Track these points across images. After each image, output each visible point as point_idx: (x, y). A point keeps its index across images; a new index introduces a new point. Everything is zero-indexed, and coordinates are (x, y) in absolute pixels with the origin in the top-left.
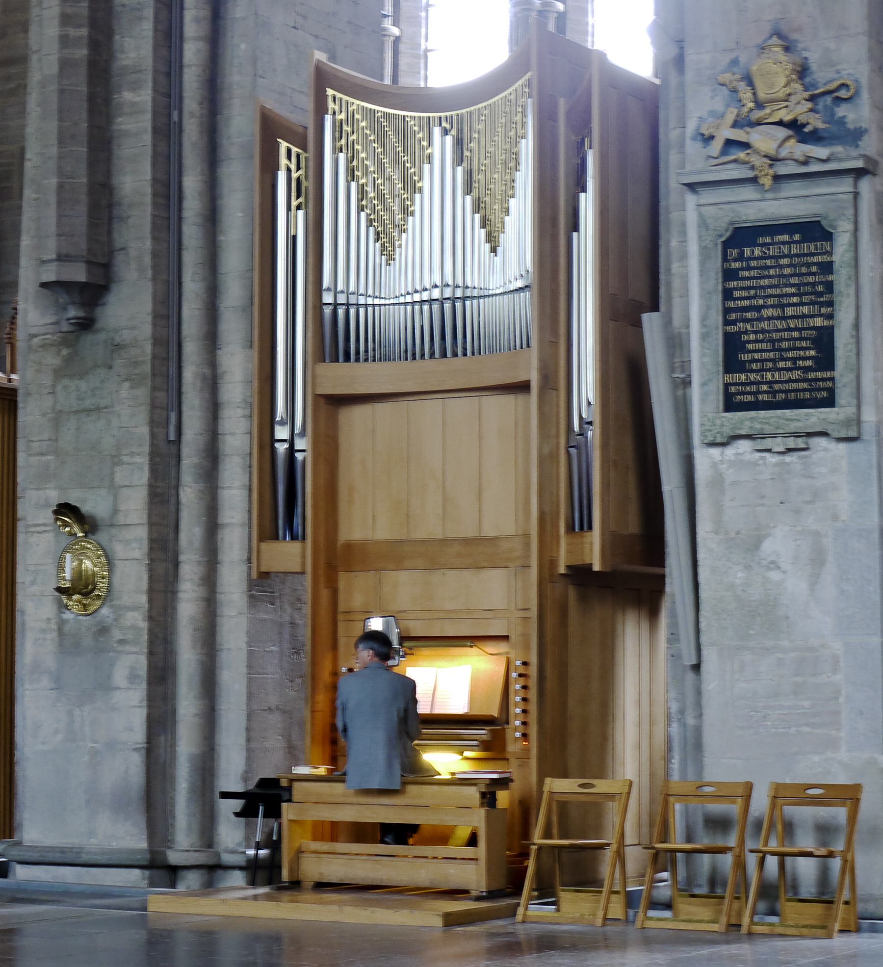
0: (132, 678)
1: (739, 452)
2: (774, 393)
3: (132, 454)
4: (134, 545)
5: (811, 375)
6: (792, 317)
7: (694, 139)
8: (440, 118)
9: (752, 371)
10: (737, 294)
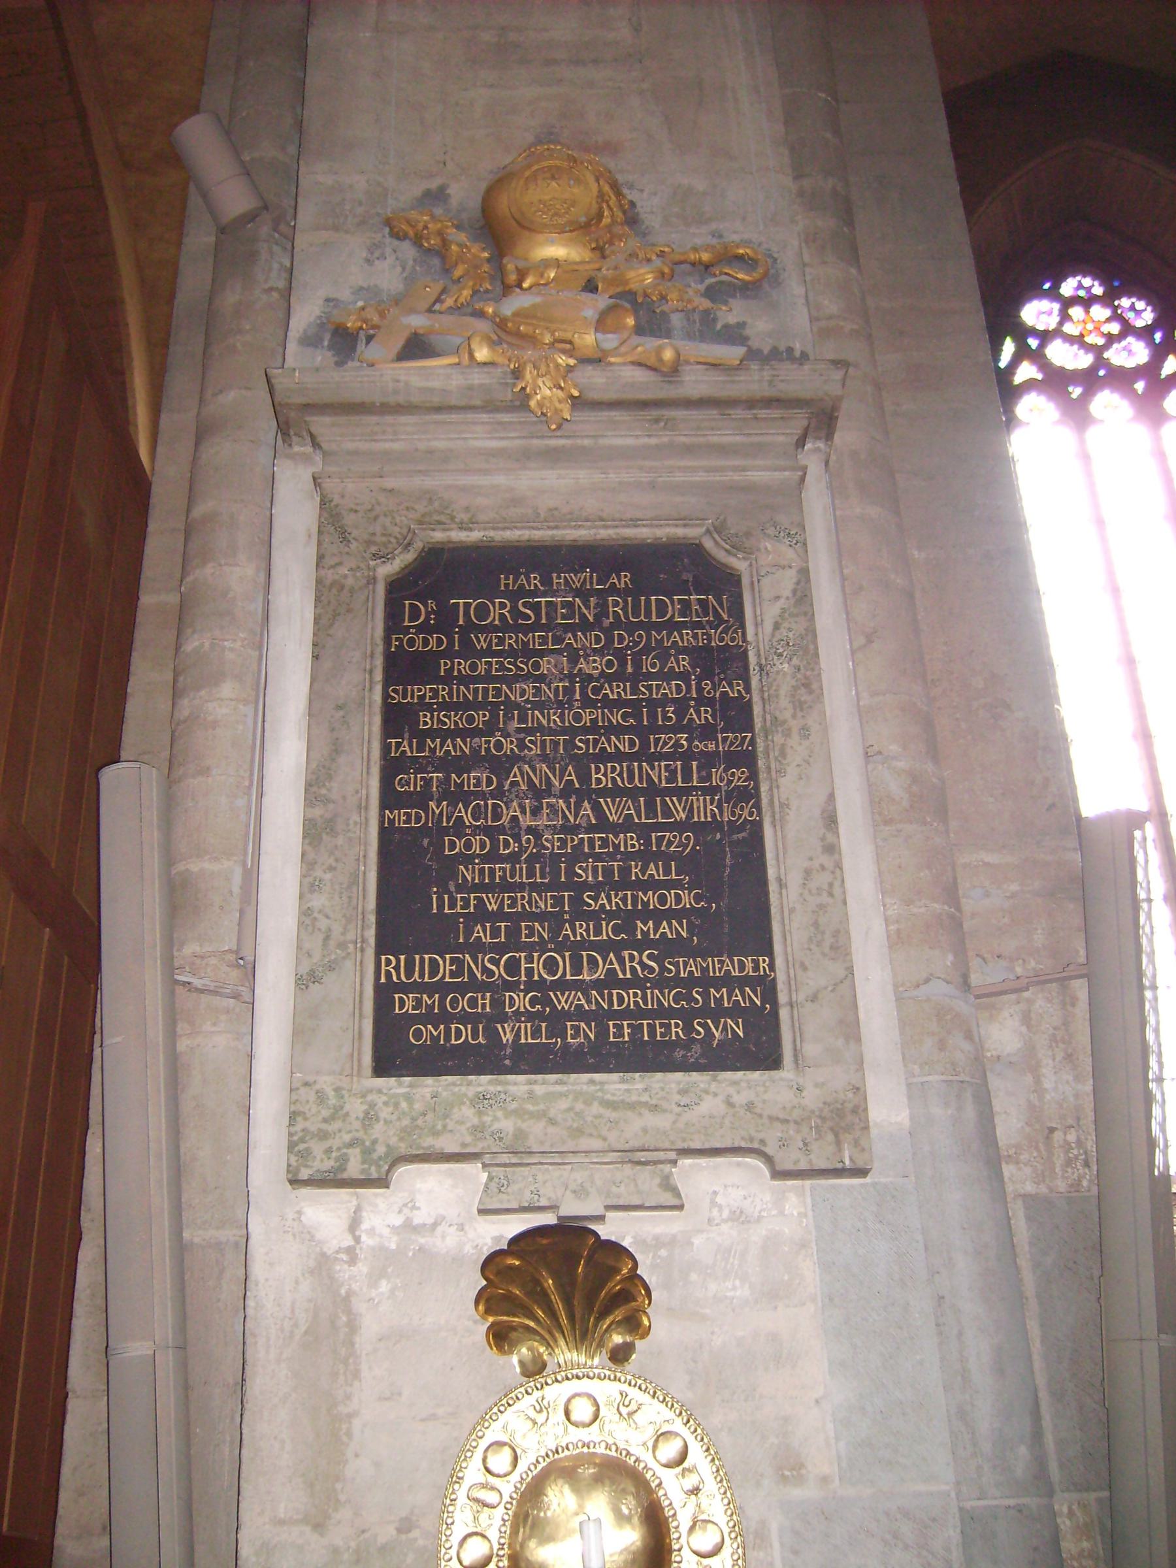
1: (417, 1221)
2: (557, 1021)
9: (477, 948)
10: (426, 720)
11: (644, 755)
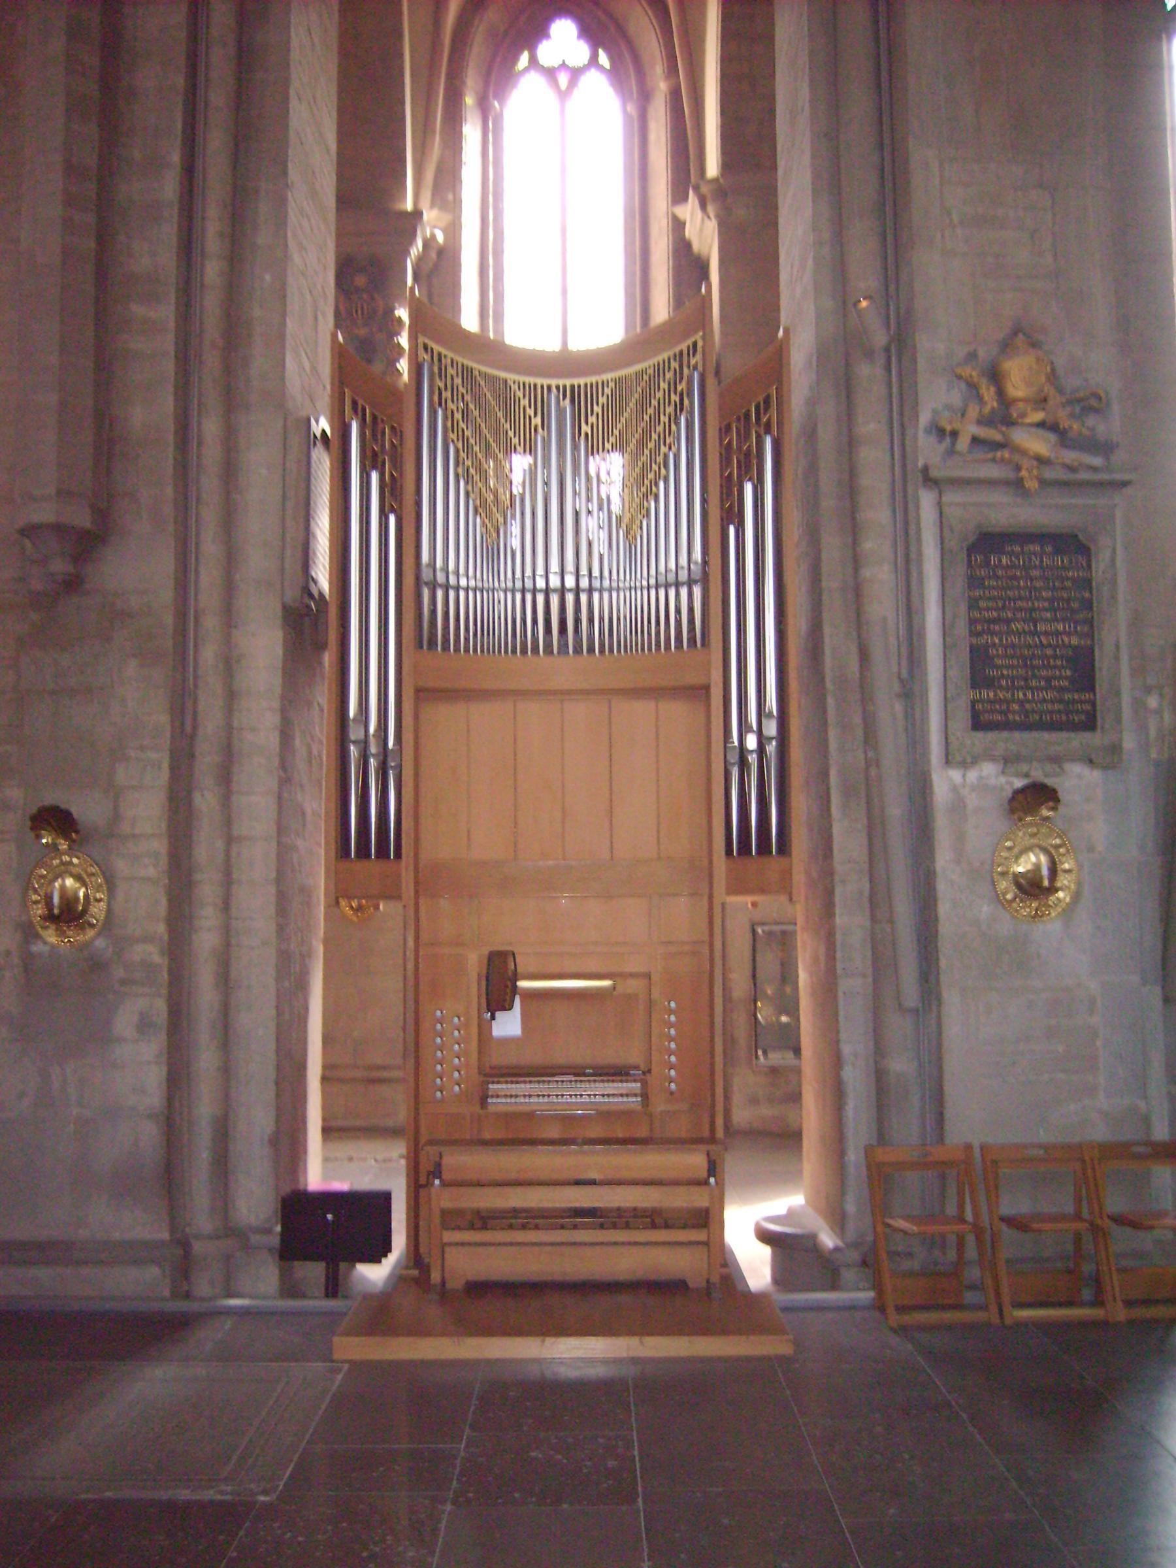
0: (144, 1025)
3: (142, 748)
4: (146, 861)
5: (1067, 696)
6: (1046, 633)
7: (928, 431)
8: (549, 388)
9: (1001, 687)
11: (1055, 620)
